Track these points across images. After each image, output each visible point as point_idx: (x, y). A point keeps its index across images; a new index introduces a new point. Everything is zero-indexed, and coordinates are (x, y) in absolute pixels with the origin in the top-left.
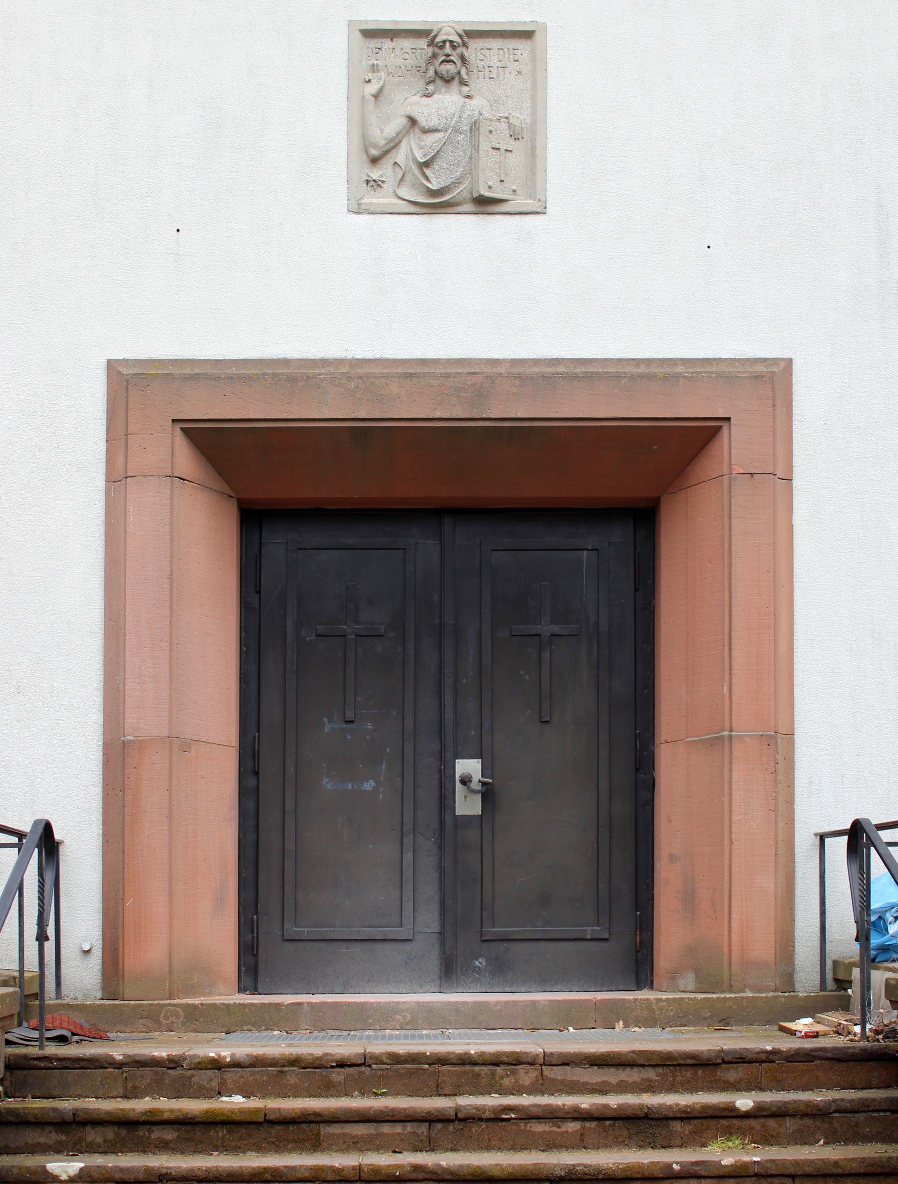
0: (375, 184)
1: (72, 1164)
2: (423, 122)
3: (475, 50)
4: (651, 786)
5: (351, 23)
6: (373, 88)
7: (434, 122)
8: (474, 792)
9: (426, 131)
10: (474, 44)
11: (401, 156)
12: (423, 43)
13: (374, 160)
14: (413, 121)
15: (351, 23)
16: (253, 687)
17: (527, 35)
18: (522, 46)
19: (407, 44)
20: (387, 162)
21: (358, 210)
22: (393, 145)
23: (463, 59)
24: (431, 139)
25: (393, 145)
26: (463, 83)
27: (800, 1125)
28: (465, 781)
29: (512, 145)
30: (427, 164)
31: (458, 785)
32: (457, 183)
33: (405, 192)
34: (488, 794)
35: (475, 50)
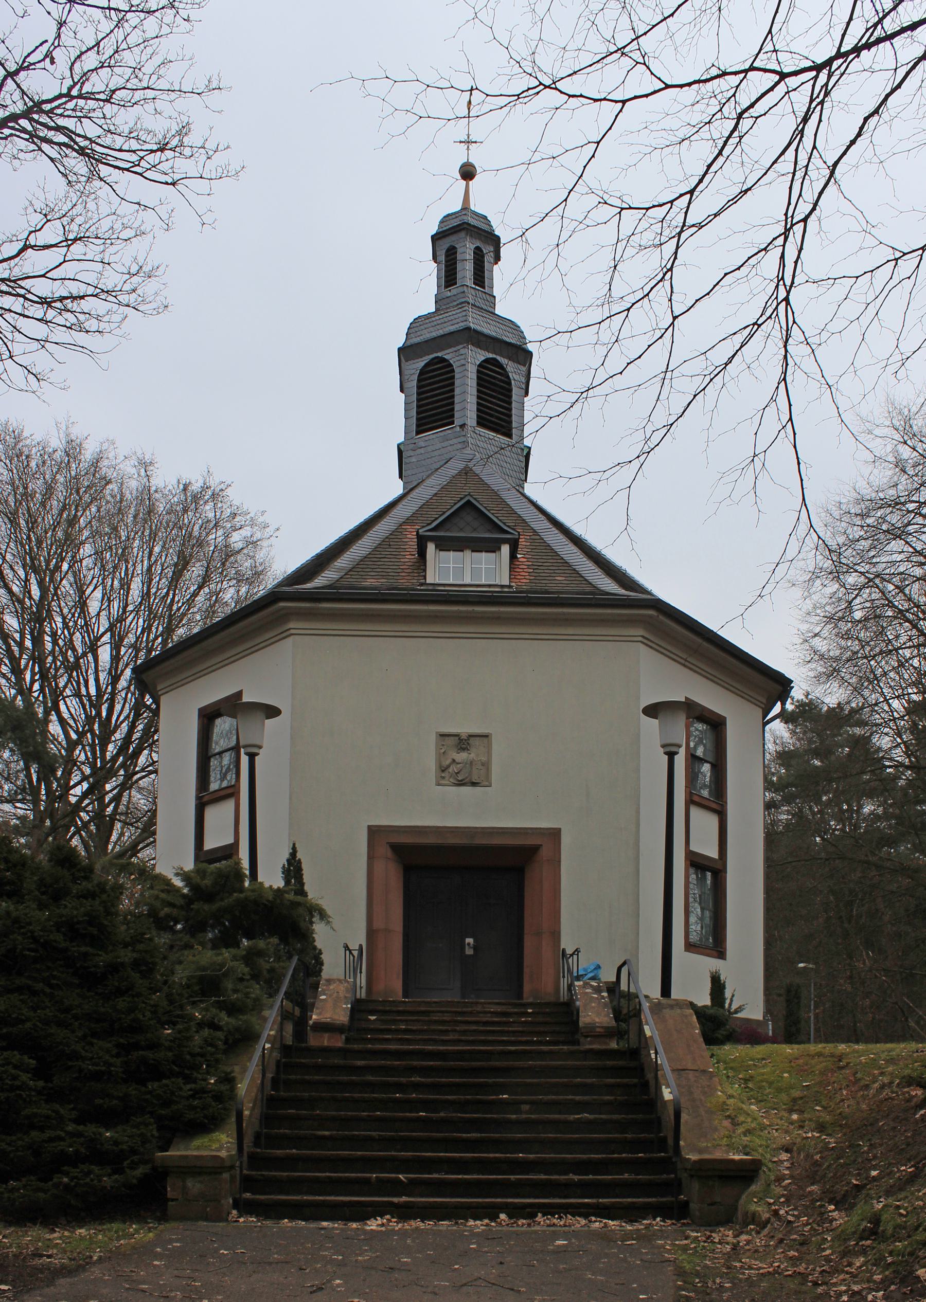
0: (443, 778)
1: (218, 1224)
2: (457, 761)
3: (472, 741)
4: (522, 947)
5: (437, 733)
6: (443, 751)
7: (460, 761)
8: (471, 948)
9: (458, 763)
10: (472, 739)
11: (450, 770)
12: (457, 738)
13: (443, 771)
14: (454, 760)
15: (437, 733)
16: (453, 231)
17: (486, 736)
18: (485, 740)
19: (452, 738)
20: (447, 771)
21: (439, 785)
22: (448, 766)
23: (468, 743)
24: (459, 766)
25: (448, 766)
26: (468, 750)
27: (79, 884)
28: (469, 944)
29: (482, 767)
30: (458, 773)
31: (467, 946)
32: (467, 778)
33: (451, 780)
34: (475, 948)
35: (472, 741)
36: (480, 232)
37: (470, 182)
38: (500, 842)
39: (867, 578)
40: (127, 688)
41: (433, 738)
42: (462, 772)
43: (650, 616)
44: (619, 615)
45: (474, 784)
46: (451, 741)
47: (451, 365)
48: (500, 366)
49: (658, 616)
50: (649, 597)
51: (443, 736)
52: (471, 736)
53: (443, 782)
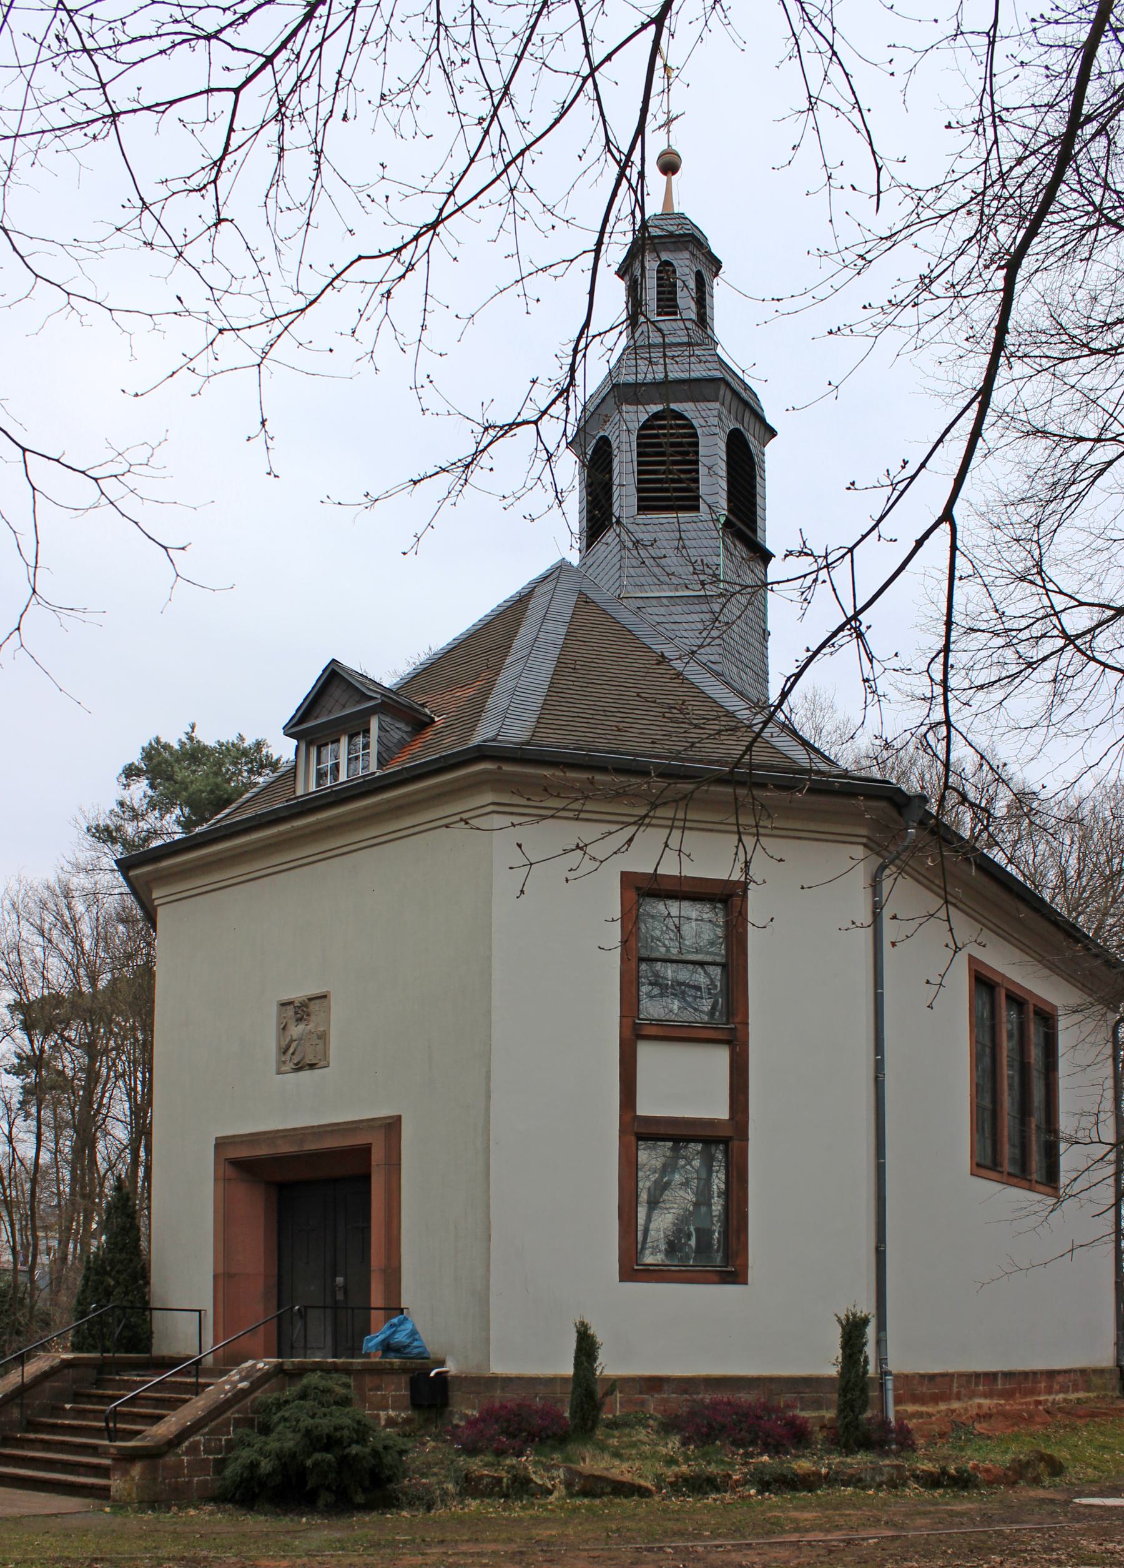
17: (325, 997)
21: (278, 1073)
36: (663, 240)
37: (674, 178)
38: (313, 1147)
39: (1089, 119)
40: (77, 922)
41: (274, 1010)
42: (297, 1053)
43: (488, 772)
44: (456, 780)
45: (312, 1066)
46: (290, 1011)
47: (695, 435)
48: (680, 416)
49: (500, 768)
50: (753, 537)
51: (284, 1004)
52: (310, 999)
53: (284, 1068)
